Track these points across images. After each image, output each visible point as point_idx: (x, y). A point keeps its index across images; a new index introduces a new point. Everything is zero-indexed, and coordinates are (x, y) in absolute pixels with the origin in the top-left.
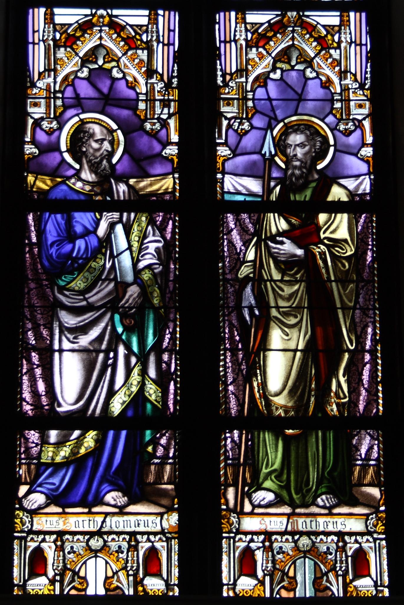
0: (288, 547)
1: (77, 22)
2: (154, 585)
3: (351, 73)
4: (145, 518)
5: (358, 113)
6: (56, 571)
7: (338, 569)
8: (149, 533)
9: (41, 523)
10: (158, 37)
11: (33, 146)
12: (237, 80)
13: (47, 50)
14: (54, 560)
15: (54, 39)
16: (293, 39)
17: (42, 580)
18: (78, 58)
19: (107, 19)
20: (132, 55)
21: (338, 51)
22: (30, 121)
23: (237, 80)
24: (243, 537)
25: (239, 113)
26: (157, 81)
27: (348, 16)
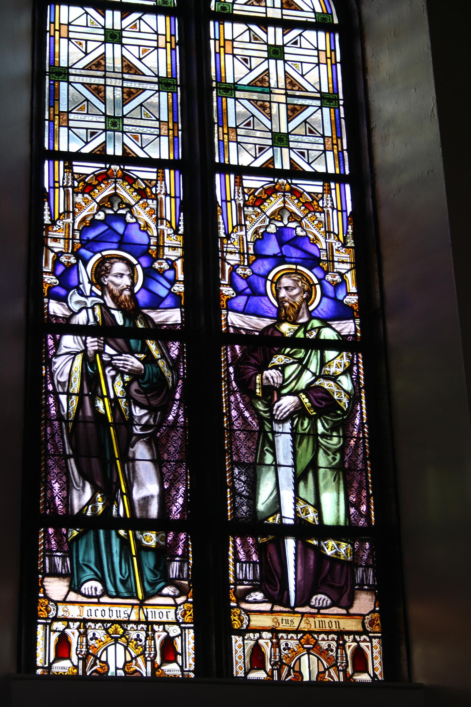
0: (293, 644)
1: (262, 187)
2: (172, 669)
7: (147, 656)
8: (164, 623)
10: (333, 204)
11: (54, 277)
14: (78, 644)
15: (245, 201)
18: (95, 203)
20: (143, 204)
22: (51, 255)
25: (240, 261)
26: (335, 241)
27: (164, 173)
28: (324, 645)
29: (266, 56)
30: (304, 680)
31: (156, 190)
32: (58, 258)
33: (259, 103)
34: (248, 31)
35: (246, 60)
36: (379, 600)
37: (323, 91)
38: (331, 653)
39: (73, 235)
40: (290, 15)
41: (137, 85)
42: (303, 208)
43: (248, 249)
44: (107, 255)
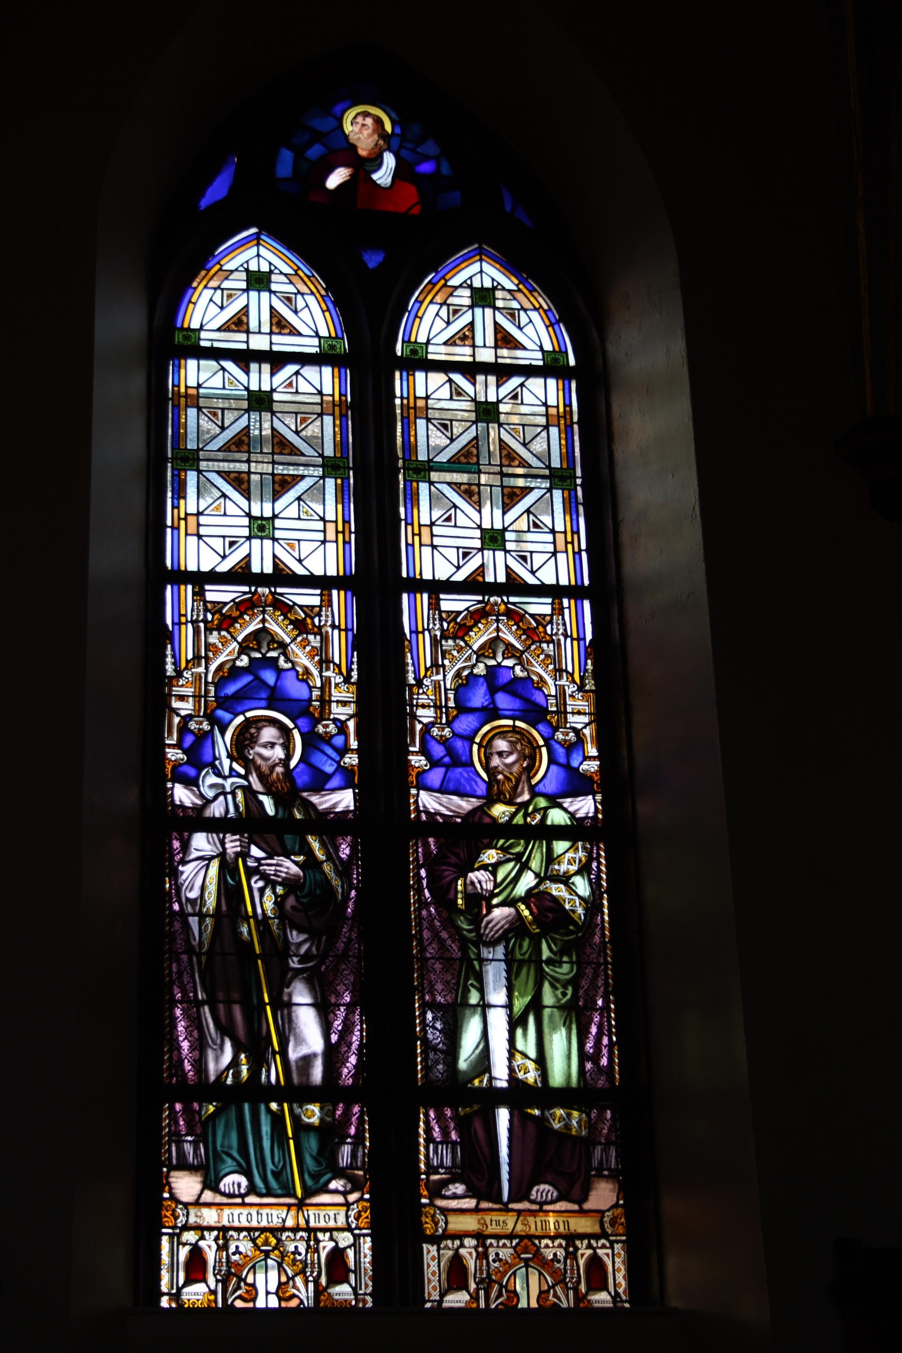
3: (335, 664)
5: (339, 712)
6: (218, 1277)
8: (331, 1230)
9: (458, 1223)
12: (193, 670)
13: (434, 639)
16: (264, 621)
17: (200, 1288)
19: (503, 607)
20: (302, 641)
25: (436, 718)
30: (520, 1306)
31: (320, 621)
34: (448, 385)
36: (624, 1190)
39: (206, 690)
40: (506, 356)
41: (292, 471)
43: (447, 699)
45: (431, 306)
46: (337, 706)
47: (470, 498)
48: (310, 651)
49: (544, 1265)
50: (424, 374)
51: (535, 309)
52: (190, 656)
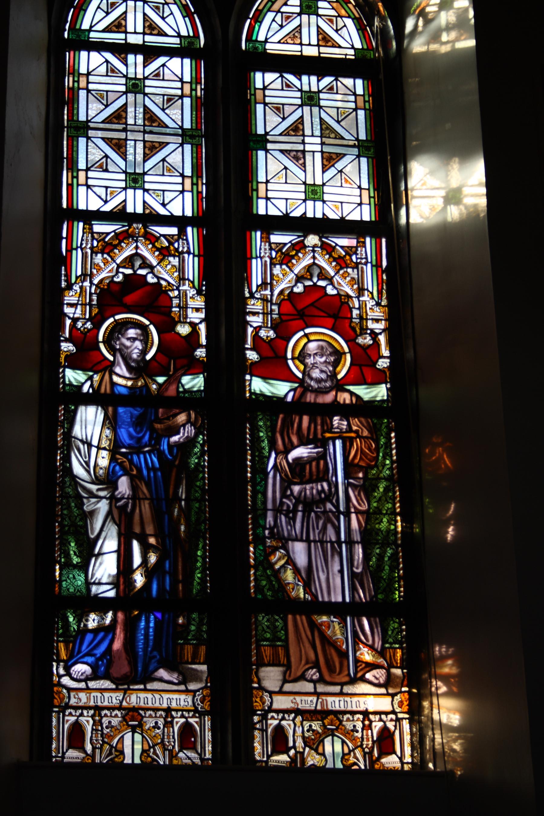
1: (290, 242)
2: (391, 761)
4: (171, 696)
5: (195, 317)
7: (364, 746)
12: (262, 292)
13: (85, 256)
15: (92, 248)
18: (114, 264)
20: (343, 273)
21: (355, 270)
22: (250, 330)
23: (262, 292)
24: (274, 715)
28: (349, 726)
29: (124, 90)
30: (125, 762)
32: (257, 333)
33: (293, 154)
34: (105, 64)
35: (278, 109)
37: (360, 138)
38: (158, 731)
42: (334, 264)
44: (121, 319)
45: (269, 13)
46: (192, 312)
47: (119, 150)
48: (350, 281)
49: (350, 734)
50: (86, 53)
51: (349, 17)
52: (79, 273)
